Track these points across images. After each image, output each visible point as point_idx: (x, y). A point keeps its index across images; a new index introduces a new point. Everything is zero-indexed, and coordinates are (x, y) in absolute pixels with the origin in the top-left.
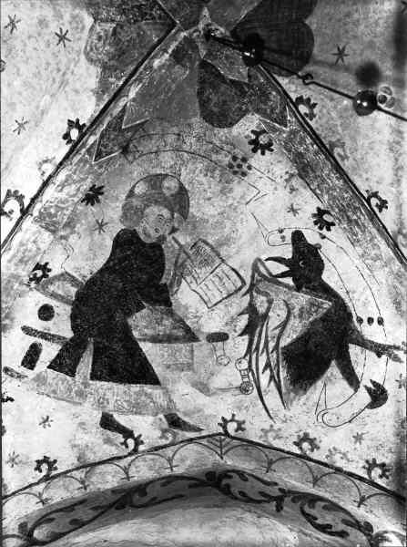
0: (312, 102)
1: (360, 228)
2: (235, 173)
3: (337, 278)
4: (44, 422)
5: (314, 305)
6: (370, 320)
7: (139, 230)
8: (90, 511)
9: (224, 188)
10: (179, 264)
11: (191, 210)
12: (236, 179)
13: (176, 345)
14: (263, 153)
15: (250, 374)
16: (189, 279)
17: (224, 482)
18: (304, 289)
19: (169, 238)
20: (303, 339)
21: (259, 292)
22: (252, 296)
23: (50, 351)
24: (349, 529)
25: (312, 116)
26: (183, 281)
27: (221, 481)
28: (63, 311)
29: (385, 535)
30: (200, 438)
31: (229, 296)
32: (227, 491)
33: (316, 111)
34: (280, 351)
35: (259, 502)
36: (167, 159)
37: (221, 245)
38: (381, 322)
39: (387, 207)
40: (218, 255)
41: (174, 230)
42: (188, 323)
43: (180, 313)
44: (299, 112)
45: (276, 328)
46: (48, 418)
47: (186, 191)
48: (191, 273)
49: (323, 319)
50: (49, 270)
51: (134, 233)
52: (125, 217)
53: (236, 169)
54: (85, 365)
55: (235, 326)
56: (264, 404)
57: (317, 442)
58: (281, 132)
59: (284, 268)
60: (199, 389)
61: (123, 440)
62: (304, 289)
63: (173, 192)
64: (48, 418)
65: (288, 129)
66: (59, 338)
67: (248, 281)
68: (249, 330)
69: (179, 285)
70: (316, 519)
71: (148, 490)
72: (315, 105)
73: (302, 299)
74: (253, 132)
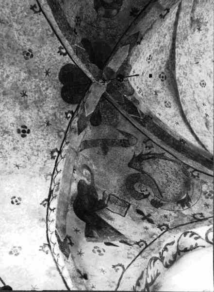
0: (59, 54)
25: (60, 48)
33: (58, 50)
39: (31, 6)
40: (193, 190)
47: (95, 8)
72: (58, 52)
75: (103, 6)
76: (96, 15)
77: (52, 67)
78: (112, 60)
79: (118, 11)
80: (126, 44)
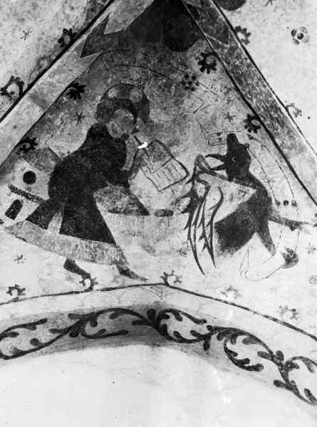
0: (247, 32)
1: (279, 123)
2: (186, 88)
3: (260, 170)
4: (19, 259)
5: (242, 191)
6: (286, 203)
7: (109, 126)
8: (49, 334)
9: (178, 100)
10: (137, 157)
11: (150, 116)
12: (187, 92)
13: (130, 217)
14: (208, 72)
15: (189, 242)
16: (145, 168)
17: (163, 322)
18: (234, 179)
19: (131, 137)
20: (232, 217)
21: (200, 181)
22: (193, 184)
23: (29, 208)
24: (264, 361)
26: (140, 170)
27: (160, 320)
28: (43, 177)
29: (294, 362)
30: (145, 285)
31: (175, 183)
32: (163, 331)
33: (250, 38)
34: (214, 225)
35: (190, 342)
36: (135, 74)
37: (171, 145)
38: (294, 204)
39: (301, 115)
40: (169, 153)
41: (136, 131)
42: (141, 201)
43: (136, 193)
44: (237, 38)
45: (211, 209)
46: (22, 256)
47: (148, 101)
48: (146, 164)
49: (249, 202)
50: (36, 144)
51: (105, 129)
52: (98, 115)
53: (187, 85)
54: (56, 223)
55: (179, 206)
56: (198, 264)
57: (240, 292)
58: (223, 48)
59: (219, 163)
60: (146, 250)
61: (81, 280)
62: (234, 179)
63: (138, 101)
64: (22, 256)
65: (228, 46)
66: (38, 199)
67: (191, 173)
68: (190, 209)
69: (137, 173)
70: (236, 355)
71: (99, 320)
73: (232, 187)
74: (202, 54)
75: (132, 104)
76: (145, 90)
77: (260, 8)
78: (145, 7)
79: (105, 96)
80: (112, 35)
